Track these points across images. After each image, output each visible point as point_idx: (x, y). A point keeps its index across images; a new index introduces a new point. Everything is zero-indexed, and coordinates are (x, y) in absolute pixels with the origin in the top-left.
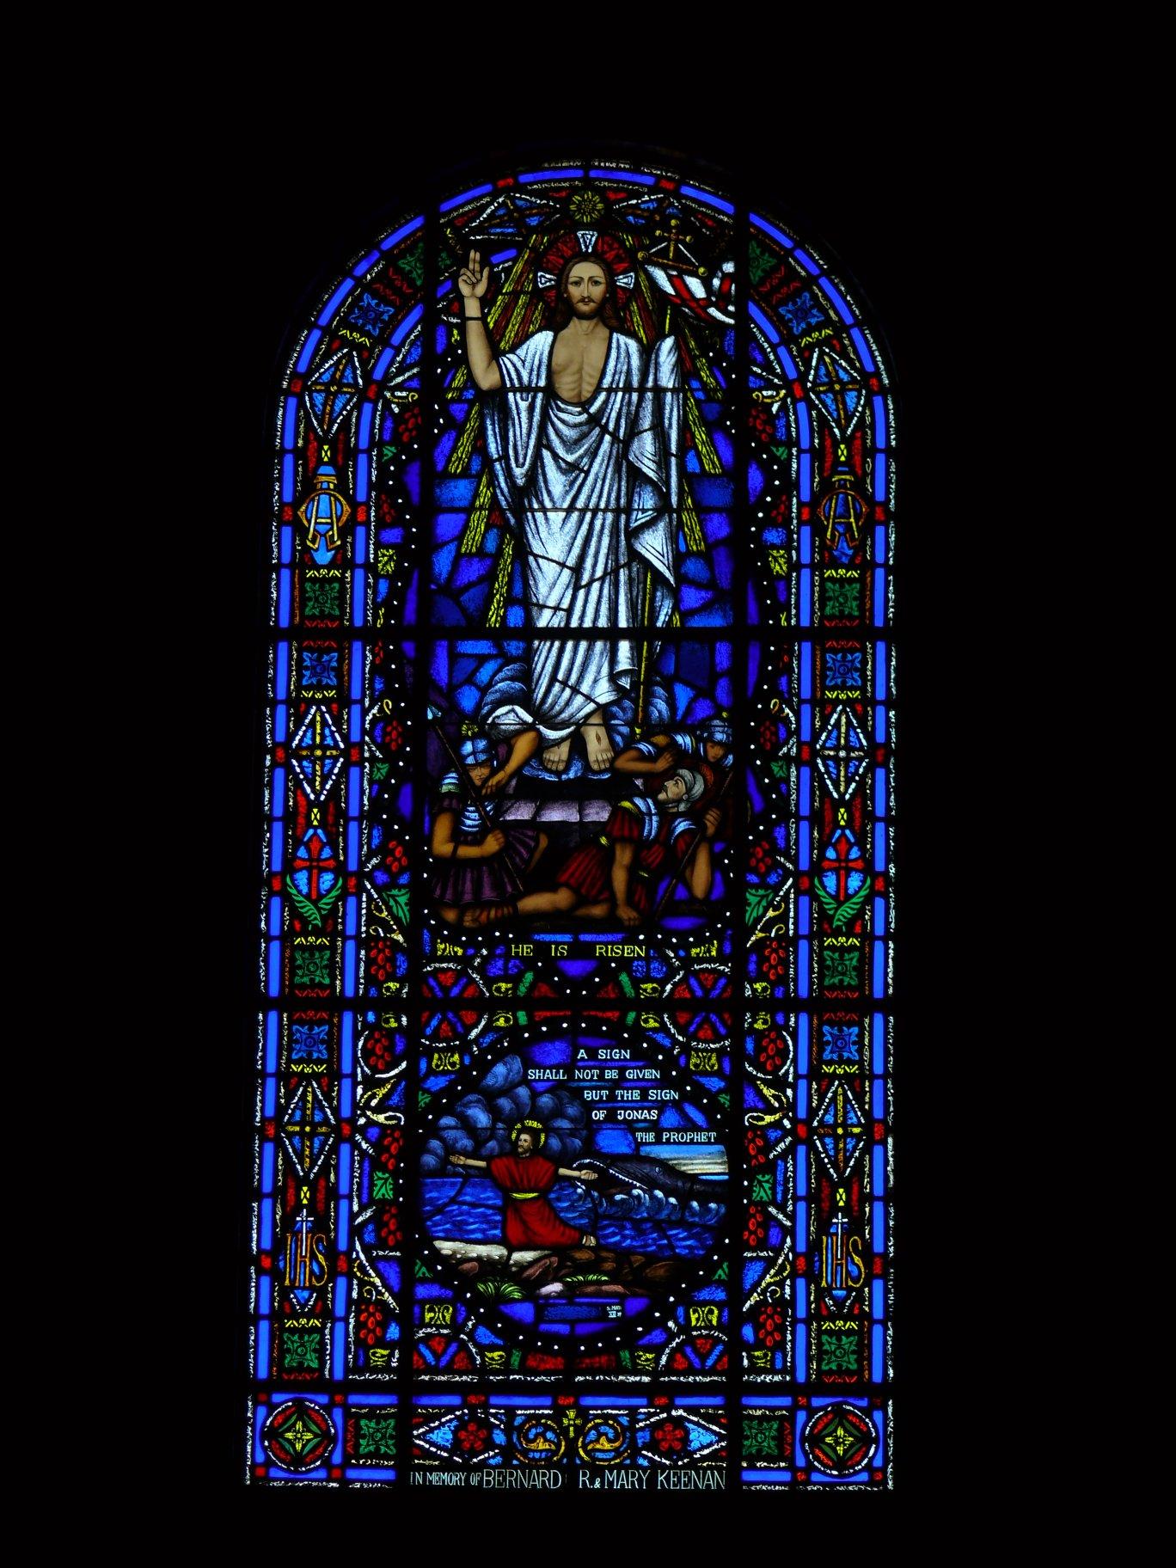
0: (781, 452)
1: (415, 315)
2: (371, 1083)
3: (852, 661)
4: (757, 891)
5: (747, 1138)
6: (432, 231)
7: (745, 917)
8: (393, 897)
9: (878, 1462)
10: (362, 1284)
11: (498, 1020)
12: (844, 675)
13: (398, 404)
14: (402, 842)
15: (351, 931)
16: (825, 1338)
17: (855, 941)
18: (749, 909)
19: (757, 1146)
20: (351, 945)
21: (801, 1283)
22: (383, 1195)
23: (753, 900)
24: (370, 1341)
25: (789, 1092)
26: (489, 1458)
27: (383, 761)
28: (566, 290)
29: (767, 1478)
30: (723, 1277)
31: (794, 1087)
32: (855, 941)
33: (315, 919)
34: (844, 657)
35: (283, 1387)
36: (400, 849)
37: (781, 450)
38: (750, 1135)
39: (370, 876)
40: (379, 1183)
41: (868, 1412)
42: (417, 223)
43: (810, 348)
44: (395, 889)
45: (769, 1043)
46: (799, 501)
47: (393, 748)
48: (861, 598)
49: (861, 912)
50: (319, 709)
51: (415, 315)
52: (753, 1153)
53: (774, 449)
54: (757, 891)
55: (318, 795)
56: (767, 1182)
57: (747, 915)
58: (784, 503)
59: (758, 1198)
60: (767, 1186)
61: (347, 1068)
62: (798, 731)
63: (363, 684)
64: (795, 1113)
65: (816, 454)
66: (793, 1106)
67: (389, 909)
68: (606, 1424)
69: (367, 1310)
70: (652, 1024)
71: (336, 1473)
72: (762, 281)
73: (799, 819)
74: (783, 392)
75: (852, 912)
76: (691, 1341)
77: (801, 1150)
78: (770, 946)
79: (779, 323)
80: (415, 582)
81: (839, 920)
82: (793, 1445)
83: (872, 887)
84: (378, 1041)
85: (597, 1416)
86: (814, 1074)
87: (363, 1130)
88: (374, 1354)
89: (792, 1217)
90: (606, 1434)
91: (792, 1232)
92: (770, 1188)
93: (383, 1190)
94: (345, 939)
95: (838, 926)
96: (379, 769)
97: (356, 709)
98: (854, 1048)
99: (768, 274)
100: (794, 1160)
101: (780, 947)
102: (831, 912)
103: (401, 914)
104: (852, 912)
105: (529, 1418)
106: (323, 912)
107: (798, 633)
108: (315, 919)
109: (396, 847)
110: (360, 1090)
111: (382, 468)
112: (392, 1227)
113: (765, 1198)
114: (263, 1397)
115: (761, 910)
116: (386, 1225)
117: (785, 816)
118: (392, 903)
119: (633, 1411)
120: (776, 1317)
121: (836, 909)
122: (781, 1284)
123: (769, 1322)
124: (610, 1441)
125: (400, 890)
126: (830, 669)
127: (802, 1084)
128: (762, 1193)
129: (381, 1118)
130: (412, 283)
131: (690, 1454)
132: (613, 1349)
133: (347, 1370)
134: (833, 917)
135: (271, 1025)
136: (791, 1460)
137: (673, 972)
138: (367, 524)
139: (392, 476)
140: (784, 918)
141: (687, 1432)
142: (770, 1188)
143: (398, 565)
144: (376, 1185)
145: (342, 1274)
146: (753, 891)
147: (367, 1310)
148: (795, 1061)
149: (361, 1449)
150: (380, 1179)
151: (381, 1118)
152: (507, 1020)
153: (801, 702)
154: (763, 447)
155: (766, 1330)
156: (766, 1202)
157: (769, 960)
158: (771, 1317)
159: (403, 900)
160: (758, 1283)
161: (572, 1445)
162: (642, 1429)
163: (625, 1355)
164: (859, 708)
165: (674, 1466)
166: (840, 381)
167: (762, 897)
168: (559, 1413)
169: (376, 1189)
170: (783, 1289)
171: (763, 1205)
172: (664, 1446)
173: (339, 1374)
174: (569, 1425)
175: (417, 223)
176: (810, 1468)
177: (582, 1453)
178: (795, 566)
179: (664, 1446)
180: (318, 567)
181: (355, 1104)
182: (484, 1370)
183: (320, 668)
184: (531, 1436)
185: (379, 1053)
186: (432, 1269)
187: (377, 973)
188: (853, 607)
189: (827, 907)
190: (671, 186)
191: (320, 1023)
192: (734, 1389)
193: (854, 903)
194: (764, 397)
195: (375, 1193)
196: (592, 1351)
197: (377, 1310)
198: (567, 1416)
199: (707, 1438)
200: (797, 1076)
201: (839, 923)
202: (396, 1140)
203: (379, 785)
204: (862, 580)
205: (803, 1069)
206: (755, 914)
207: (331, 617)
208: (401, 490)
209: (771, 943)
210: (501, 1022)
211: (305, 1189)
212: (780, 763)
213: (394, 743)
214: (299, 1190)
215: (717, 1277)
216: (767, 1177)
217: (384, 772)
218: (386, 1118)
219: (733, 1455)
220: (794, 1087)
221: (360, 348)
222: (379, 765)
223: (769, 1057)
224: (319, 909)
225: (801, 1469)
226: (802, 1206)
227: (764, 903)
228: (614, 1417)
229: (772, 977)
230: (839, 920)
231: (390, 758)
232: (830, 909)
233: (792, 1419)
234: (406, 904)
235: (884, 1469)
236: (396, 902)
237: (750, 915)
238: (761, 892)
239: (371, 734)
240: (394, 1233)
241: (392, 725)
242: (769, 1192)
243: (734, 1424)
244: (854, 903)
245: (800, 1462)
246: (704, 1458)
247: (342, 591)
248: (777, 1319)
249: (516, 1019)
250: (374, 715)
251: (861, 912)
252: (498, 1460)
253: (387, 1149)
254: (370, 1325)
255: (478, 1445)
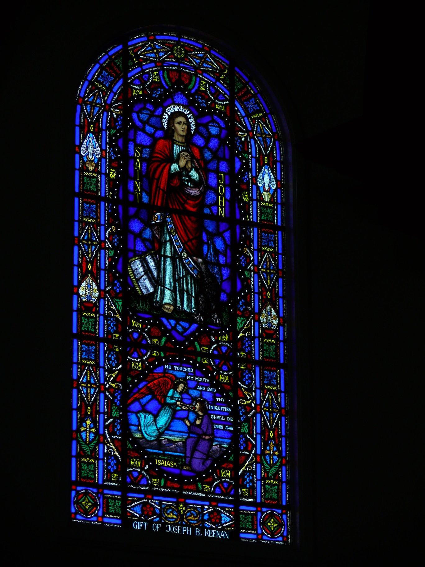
0: (245, 155)
1: (121, 82)
2: (111, 371)
3: (271, 237)
4: (241, 318)
5: (240, 443)
6: (125, 51)
7: (237, 327)
8: (117, 302)
9: (285, 534)
10: (108, 448)
11: (153, 353)
12: (268, 242)
13: (116, 114)
14: (119, 281)
15: (102, 312)
16: (267, 486)
17: (276, 482)
18: (238, 324)
19: (243, 412)
20: (102, 318)
21: (259, 465)
22: (116, 415)
23: (239, 321)
24: (112, 471)
25: (254, 394)
26: (154, 518)
27: (112, 249)
28: (174, 126)
29: (247, 536)
30: (232, 460)
31: (255, 392)
32: (276, 482)
33: (88, 452)
34: (268, 235)
35: (82, 484)
36: (118, 284)
37: (246, 155)
38: (240, 408)
39: (108, 292)
40: (114, 410)
41: (282, 535)
42: (120, 47)
43: (255, 119)
44: (118, 299)
45: (247, 477)
46: (252, 175)
47: (116, 245)
48: (275, 351)
49: (278, 471)
50: (89, 226)
51: (121, 82)
52: (241, 414)
53: (243, 154)
54: (241, 318)
55: (90, 259)
56: (246, 425)
57: (238, 326)
58: (247, 175)
59: (243, 431)
60: (246, 427)
61: (102, 364)
62: (253, 260)
63: (105, 208)
64: (256, 402)
65: (257, 160)
66: (255, 398)
67: (115, 306)
68: (193, 510)
69: (110, 320)
70: (206, 362)
71: (100, 519)
72: (238, 92)
73: (254, 293)
74: (246, 134)
75: (275, 471)
76: (222, 482)
77: (258, 416)
78: (245, 339)
79: (245, 108)
80: (121, 188)
81: (271, 474)
82: (257, 525)
83: (281, 461)
84: (112, 355)
85: (190, 507)
86: (262, 388)
87: (107, 390)
88: (113, 475)
89: (255, 439)
90: (193, 515)
91: (255, 445)
92: (247, 428)
93: (115, 413)
94: (100, 315)
95: (271, 476)
96: (111, 252)
97: (103, 228)
98: (275, 381)
99: (240, 90)
100: (256, 418)
101: (249, 340)
102: (268, 471)
103: (120, 309)
104: (275, 471)
105: (167, 505)
106: (91, 449)
107: (253, 224)
108: (88, 452)
109: (117, 283)
110: (106, 373)
111: (110, 138)
112: (118, 428)
113: (246, 432)
114: (73, 516)
115: (242, 326)
116: (116, 426)
117: (250, 292)
118: (116, 304)
119: (202, 506)
120: (250, 477)
121: (270, 469)
122: (252, 465)
123: (247, 375)
124: (195, 517)
125: (119, 300)
126: (264, 239)
127: (258, 391)
128: (245, 429)
129: (113, 385)
130: (119, 69)
131: (222, 525)
132: (195, 482)
133: (104, 481)
134: (269, 472)
135: (76, 344)
136: (256, 530)
137: (213, 343)
138: (106, 158)
139: (114, 141)
140: (250, 329)
141: (222, 517)
142: (247, 428)
143: (117, 176)
144: (113, 411)
145: (101, 443)
146: (239, 318)
147: (110, 320)
148: (255, 383)
149: (110, 510)
150: (114, 409)
151: (113, 385)
152: (157, 354)
153: (254, 249)
154: (240, 153)
155: (246, 378)
156: (246, 433)
157: (246, 480)
158: (248, 476)
159: (120, 303)
160: (242, 328)
161: (182, 516)
162: (206, 513)
163: (200, 486)
164: (276, 393)
165: (216, 529)
166: (264, 133)
167: (243, 320)
168: (178, 504)
169: (113, 413)
170: (253, 467)
171: (244, 434)
172: (213, 520)
173: (101, 482)
174: (181, 510)
175: (120, 47)
176: (263, 534)
177: (185, 520)
178: (251, 199)
179: (213, 520)
180: (89, 172)
181: (105, 379)
182: (152, 486)
183: (88, 352)
184: (169, 512)
185: (113, 360)
186: (133, 445)
187: (111, 469)
188: (272, 355)
189: (267, 468)
190: (207, 49)
191: (92, 345)
192: (237, 503)
193: (275, 468)
194: (240, 134)
195: (113, 414)
196: (189, 483)
197: (114, 459)
198: (180, 506)
199: (228, 519)
200: (256, 388)
201: (271, 475)
202: (119, 394)
203: (112, 259)
204: (276, 344)
205: (258, 386)
206: (240, 327)
207: (91, 478)
208: (115, 267)
209: (247, 474)
210: (154, 354)
211: (89, 413)
212: (248, 272)
213: (116, 243)
214: (87, 265)
215: (230, 459)
216: (246, 424)
217: (113, 253)
218: (116, 385)
219: (237, 524)
220: (255, 392)
221: (103, 90)
222: (111, 251)
223: (246, 380)
224: (90, 447)
225: (260, 534)
226: (259, 436)
227: (243, 323)
228: (196, 508)
229: (246, 351)
230: (271, 474)
231: (114, 248)
232: (268, 469)
233: (256, 515)
234: (121, 305)
235: (287, 536)
236: (118, 304)
237: (239, 326)
238: (242, 319)
239: (108, 239)
240: (119, 288)
241: (115, 236)
242: (247, 429)
243: (236, 513)
244: (275, 468)
245: (260, 532)
246: (227, 526)
247: (95, 322)
248: (251, 478)
249: (160, 354)
250: (109, 232)
251: (278, 471)
252: (158, 519)
253: (116, 397)
254: (112, 464)
255: (150, 513)
